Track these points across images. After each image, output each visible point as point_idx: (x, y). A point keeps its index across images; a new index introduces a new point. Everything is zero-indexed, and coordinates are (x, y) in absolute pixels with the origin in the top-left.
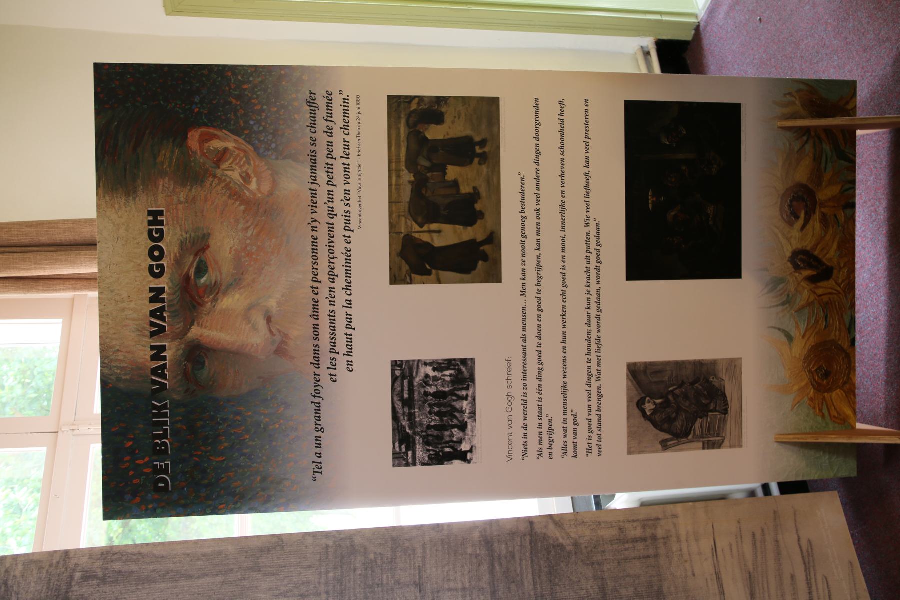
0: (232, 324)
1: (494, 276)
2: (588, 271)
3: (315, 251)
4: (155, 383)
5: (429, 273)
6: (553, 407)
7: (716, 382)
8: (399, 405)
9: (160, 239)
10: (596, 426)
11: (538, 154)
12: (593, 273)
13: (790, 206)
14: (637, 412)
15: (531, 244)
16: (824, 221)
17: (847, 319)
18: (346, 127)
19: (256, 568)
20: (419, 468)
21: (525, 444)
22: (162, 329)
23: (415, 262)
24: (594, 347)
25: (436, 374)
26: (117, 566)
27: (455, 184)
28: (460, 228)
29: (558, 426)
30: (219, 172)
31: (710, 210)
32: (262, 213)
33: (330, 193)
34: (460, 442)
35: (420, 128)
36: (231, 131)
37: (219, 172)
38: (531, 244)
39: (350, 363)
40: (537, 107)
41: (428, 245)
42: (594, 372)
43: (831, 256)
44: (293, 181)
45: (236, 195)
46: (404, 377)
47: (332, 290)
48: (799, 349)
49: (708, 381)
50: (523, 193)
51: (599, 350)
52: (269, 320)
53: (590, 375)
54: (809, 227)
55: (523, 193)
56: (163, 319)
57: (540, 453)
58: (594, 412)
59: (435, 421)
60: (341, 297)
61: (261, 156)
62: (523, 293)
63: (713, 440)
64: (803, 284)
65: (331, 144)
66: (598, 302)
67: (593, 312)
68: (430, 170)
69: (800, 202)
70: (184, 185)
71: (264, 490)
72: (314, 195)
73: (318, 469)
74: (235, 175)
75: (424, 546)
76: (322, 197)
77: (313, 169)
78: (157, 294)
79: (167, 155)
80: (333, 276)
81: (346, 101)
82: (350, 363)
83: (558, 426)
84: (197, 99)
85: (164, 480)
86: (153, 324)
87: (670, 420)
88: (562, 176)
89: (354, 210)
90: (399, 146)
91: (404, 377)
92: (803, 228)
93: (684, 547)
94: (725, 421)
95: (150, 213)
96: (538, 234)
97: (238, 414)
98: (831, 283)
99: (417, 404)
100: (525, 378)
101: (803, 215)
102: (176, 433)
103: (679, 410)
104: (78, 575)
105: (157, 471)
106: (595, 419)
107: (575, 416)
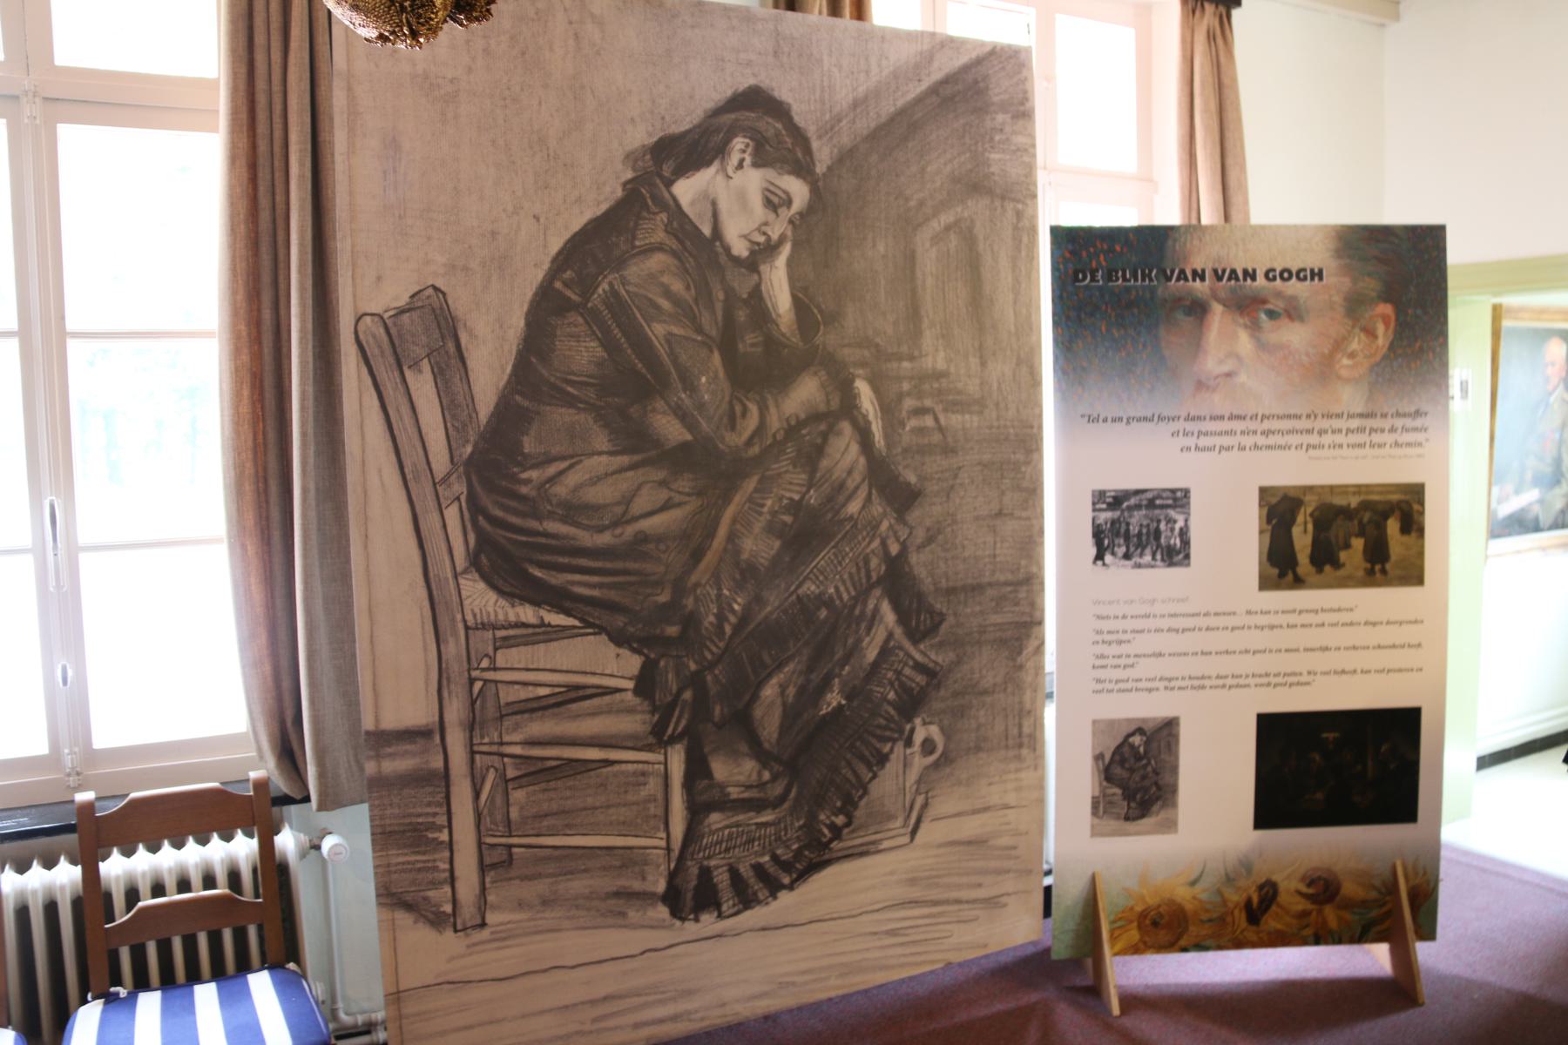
0: (1225, 342)
1: (1265, 584)
2: (1267, 675)
3: (1289, 417)
4: (1172, 272)
5: (1269, 521)
6: (1143, 644)
7: (1155, 808)
8: (1150, 495)
9: (1298, 278)
10: (1123, 688)
11: (1374, 624)
12: (1265, 680)
13: (1319, 878)
14: (1133, 727)
15: (1293, 619)
16: (1304, 914)
17: (1208, 943)
18: (1397, 444)
19: (1019, 362)
20: (1089, 514)
21: (1108, 617)
22: (1220, 278)
23: (1280, 510)
24: (1196, 683)
25: (1177, 531)
26: (1025, 239)
27: (1347, 546)
28: (1308, 551)
29: (1124, 649)
30: (1357, 330)
31: (1319, 796)
32: (1322, 370)
33: (1340, 431)
34: (1113, 554)
35: (1397, 513)
36: (1392, 344)
37: (1357, 330)
38: (1293, 619)
39: (1189, 449)
40: (1416, 622)
41: (1293, 521)
42: (1173, 684)
43: (1271, 923)
44: (1350, 398)
45: (1338, 345)
46: (1175, 499)
47: (1255, 432)
48: (1183, 894)
49: (1158, 799)
50: (1339, 610)
51: (1193, 688)
52: (1229, 375)
53: (1170, 680)
54: (1298, 898)
55: (1339, 610)
56: (1230, 279)
57: (1099, 632)
58: (1135, 685)
59: (1134, 530)
60: (1248, 441)
61: (1371, 369)
62: (1249, 612)
63: (1100, 807)
64: (1245, 896)
65: (1383, 431)
66: (1238, 686)
67: (1229, 681)
68: (1360, 522)
69: (1323, 888)
70: (1346, 299)
71: (1074, 369)
72: (1339, 416)
73: (1093, 419)
74: (1354, 345)
75: (1028, 519)
76: (1336, 423)
77: (1361, 415)
78: (1250, 275)
79: (1371, 286)
80: (1266, 433)
81: (1420, 444)
82: (1189, 449)
83: (1124, 649)
84: (1419, 312)
85: (1085, 278)
86: (1224, 271)
87: (1122, 762)
88: (1354, 648)
89: (1326, 452)
90: (1381, 493)
91: (1175, 499)
92: (1299, 893)
93: (1012, 776)
94: (1118, 818)
95: (1321, 271)
96: (1303, 626)
97: (1144, 346)
98: (1244, 923)
99: (1150, 513)
100: (1171, 616)
101: (1311, 891)
102: (1128, 290)
103: (1132, 770)
104: (1020, 206)
105: (1093, 273)
106: (1129, 685)
107: (1132, 666)
